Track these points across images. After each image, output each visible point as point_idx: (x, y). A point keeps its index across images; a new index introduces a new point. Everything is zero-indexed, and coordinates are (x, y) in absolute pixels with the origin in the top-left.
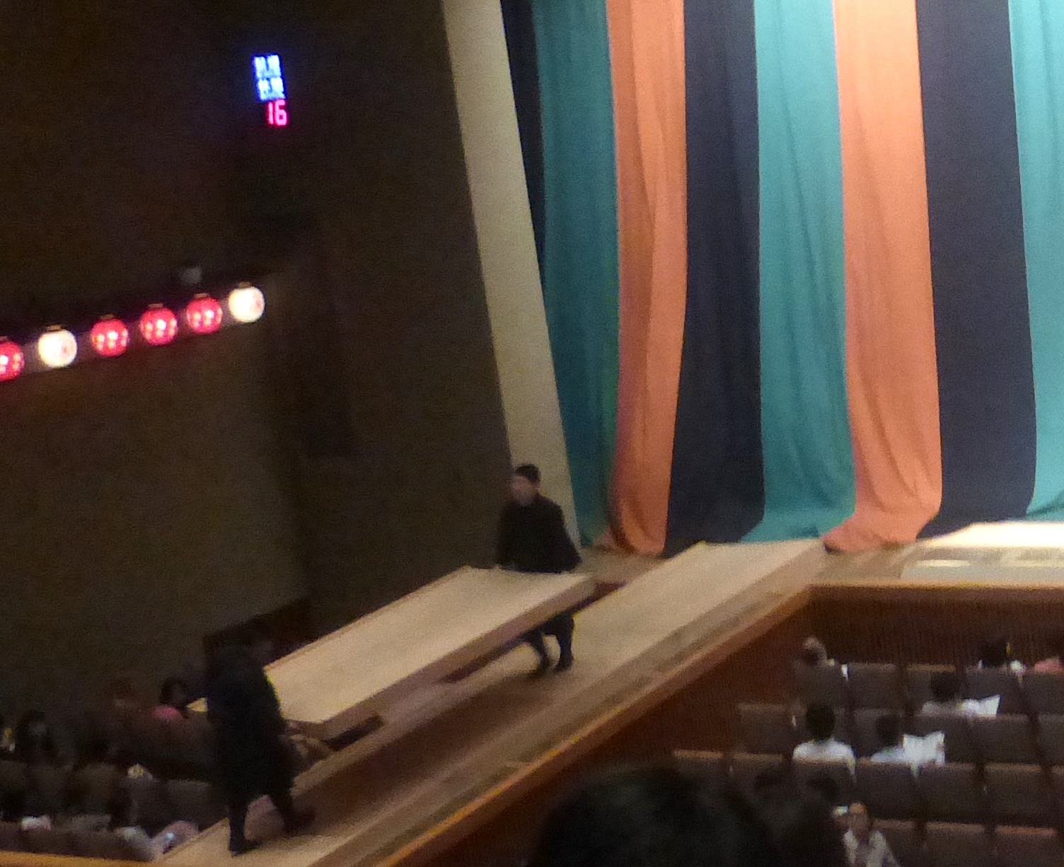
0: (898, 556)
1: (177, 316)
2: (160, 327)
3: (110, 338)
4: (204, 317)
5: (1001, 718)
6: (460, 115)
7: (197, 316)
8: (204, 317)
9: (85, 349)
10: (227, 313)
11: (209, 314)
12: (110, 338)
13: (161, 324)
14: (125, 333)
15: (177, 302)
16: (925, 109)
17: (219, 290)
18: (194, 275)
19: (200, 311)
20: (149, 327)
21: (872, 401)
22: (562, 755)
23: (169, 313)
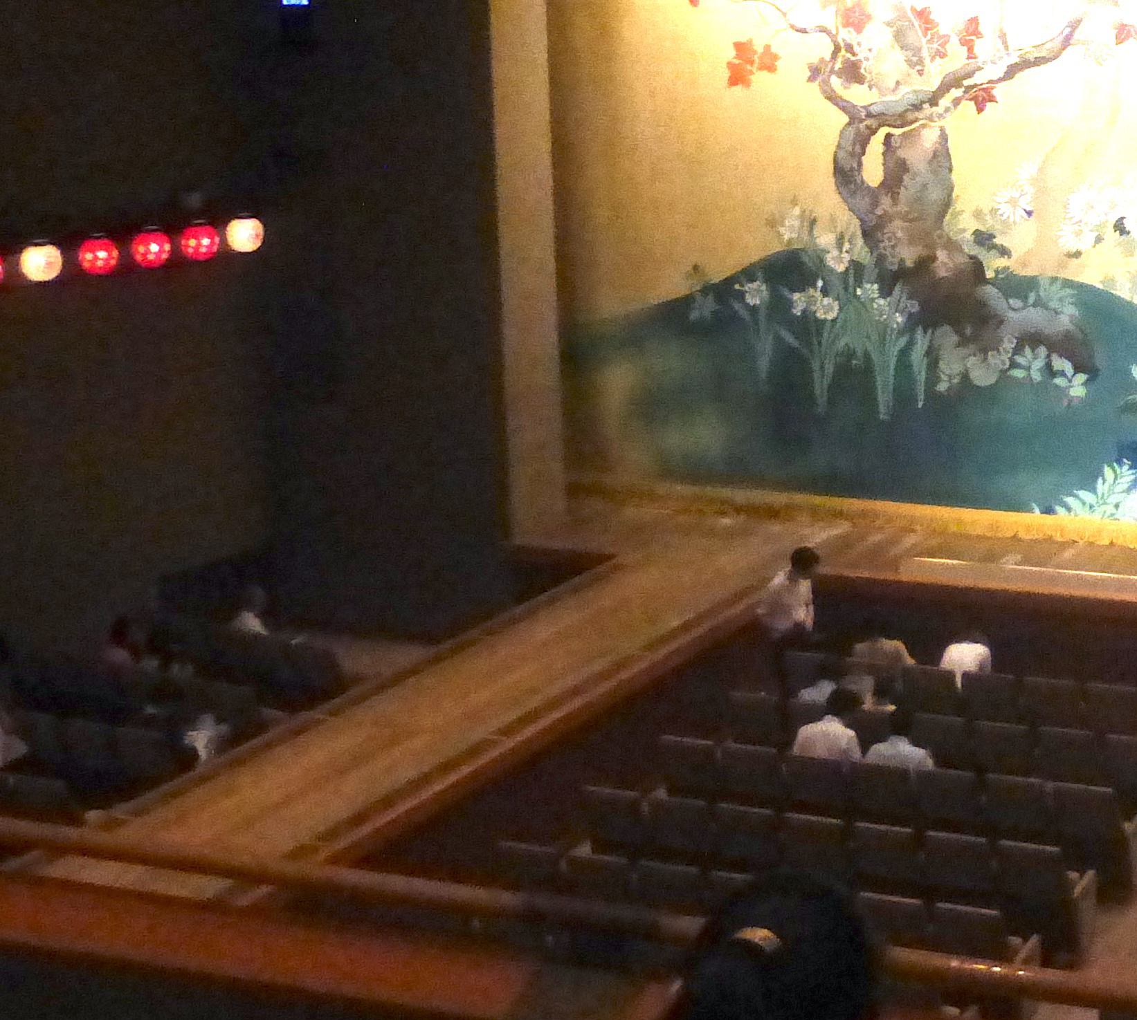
0: (229, 803)
1: (171, 242)
2: (154, 249)
3: (99, 257)
4: (201, 243)
5: (939, 770)
6: (162, 870)
7: (192, 242)
8: (201, 243)
9: (71, 264)
10: (224, 241)
11: (206, 241)
12: (99, 257)
13: (154, 248)
14: (115, 253)
15: (173, 227)
16: (948, 164)
17: (218, 221)
18: (194, 200)
19: (196, 238)
20: (141, 249)
21: (117, 855)
22: (529, 741)
23: (166, 238)
